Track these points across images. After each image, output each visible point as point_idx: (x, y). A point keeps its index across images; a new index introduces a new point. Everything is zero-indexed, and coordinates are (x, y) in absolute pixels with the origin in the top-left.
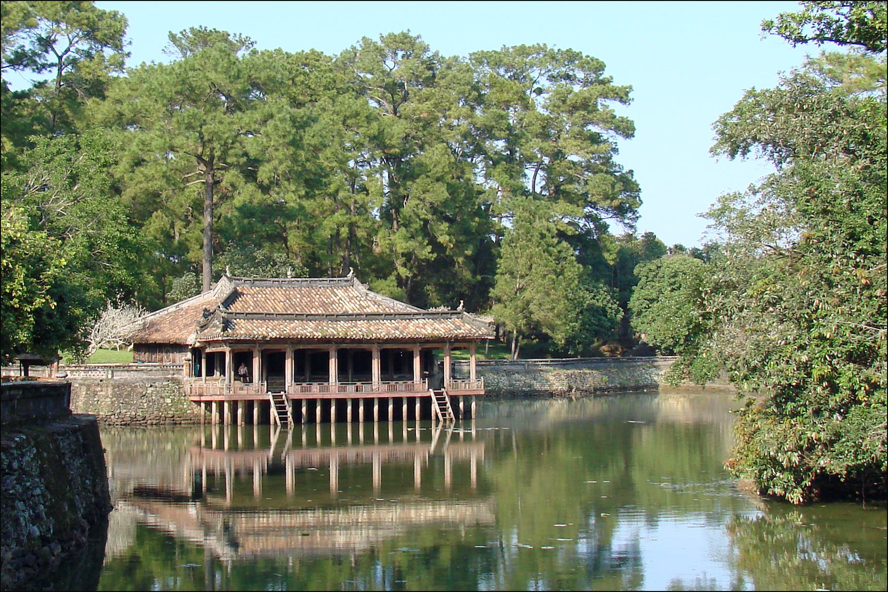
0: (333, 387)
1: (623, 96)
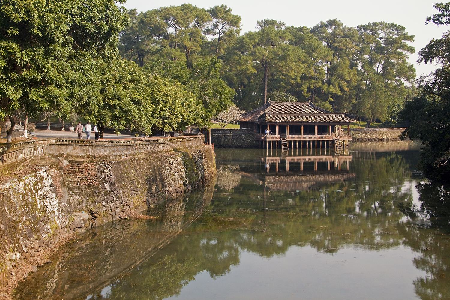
0: (302, 137)
1: (411, 38)
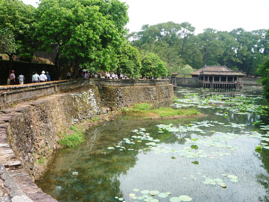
0: (220, 82)
